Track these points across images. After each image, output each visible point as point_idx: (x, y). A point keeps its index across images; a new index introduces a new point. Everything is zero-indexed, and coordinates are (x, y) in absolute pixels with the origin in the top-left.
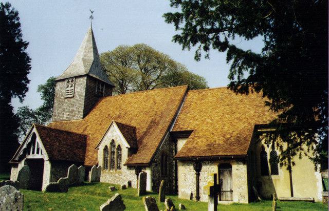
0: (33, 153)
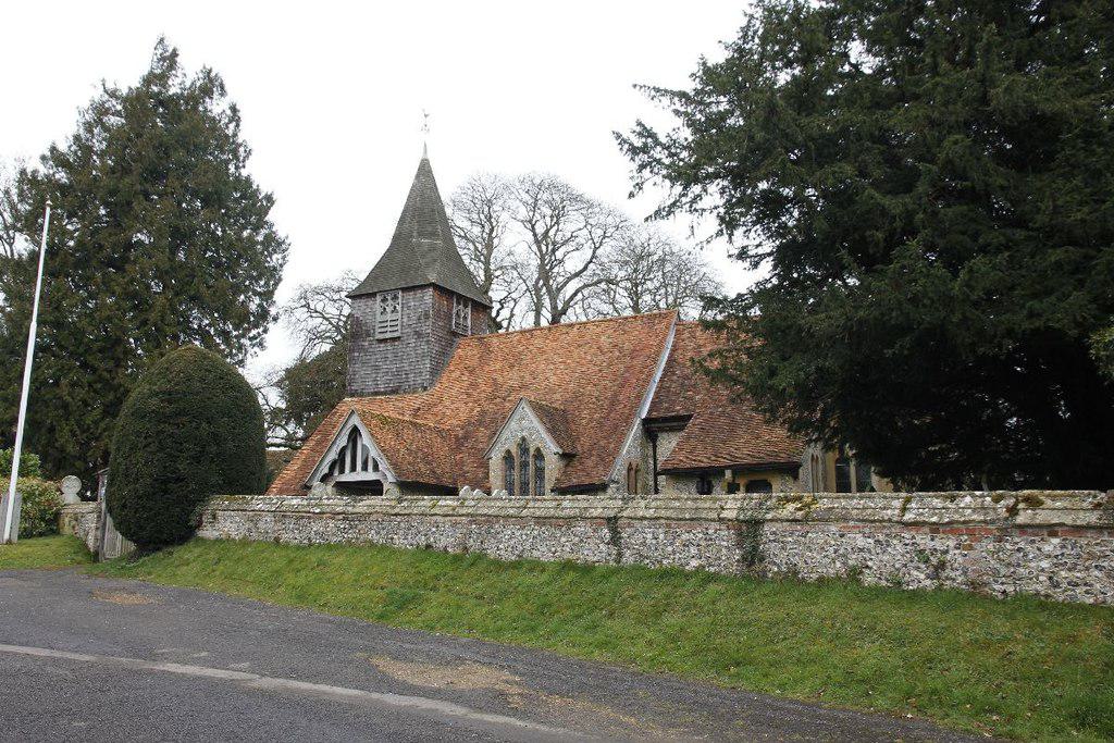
0: (353, 469)
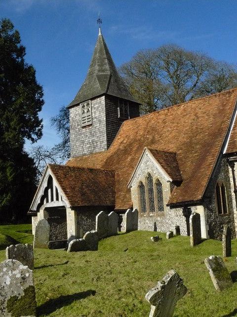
0: (52, 200)
